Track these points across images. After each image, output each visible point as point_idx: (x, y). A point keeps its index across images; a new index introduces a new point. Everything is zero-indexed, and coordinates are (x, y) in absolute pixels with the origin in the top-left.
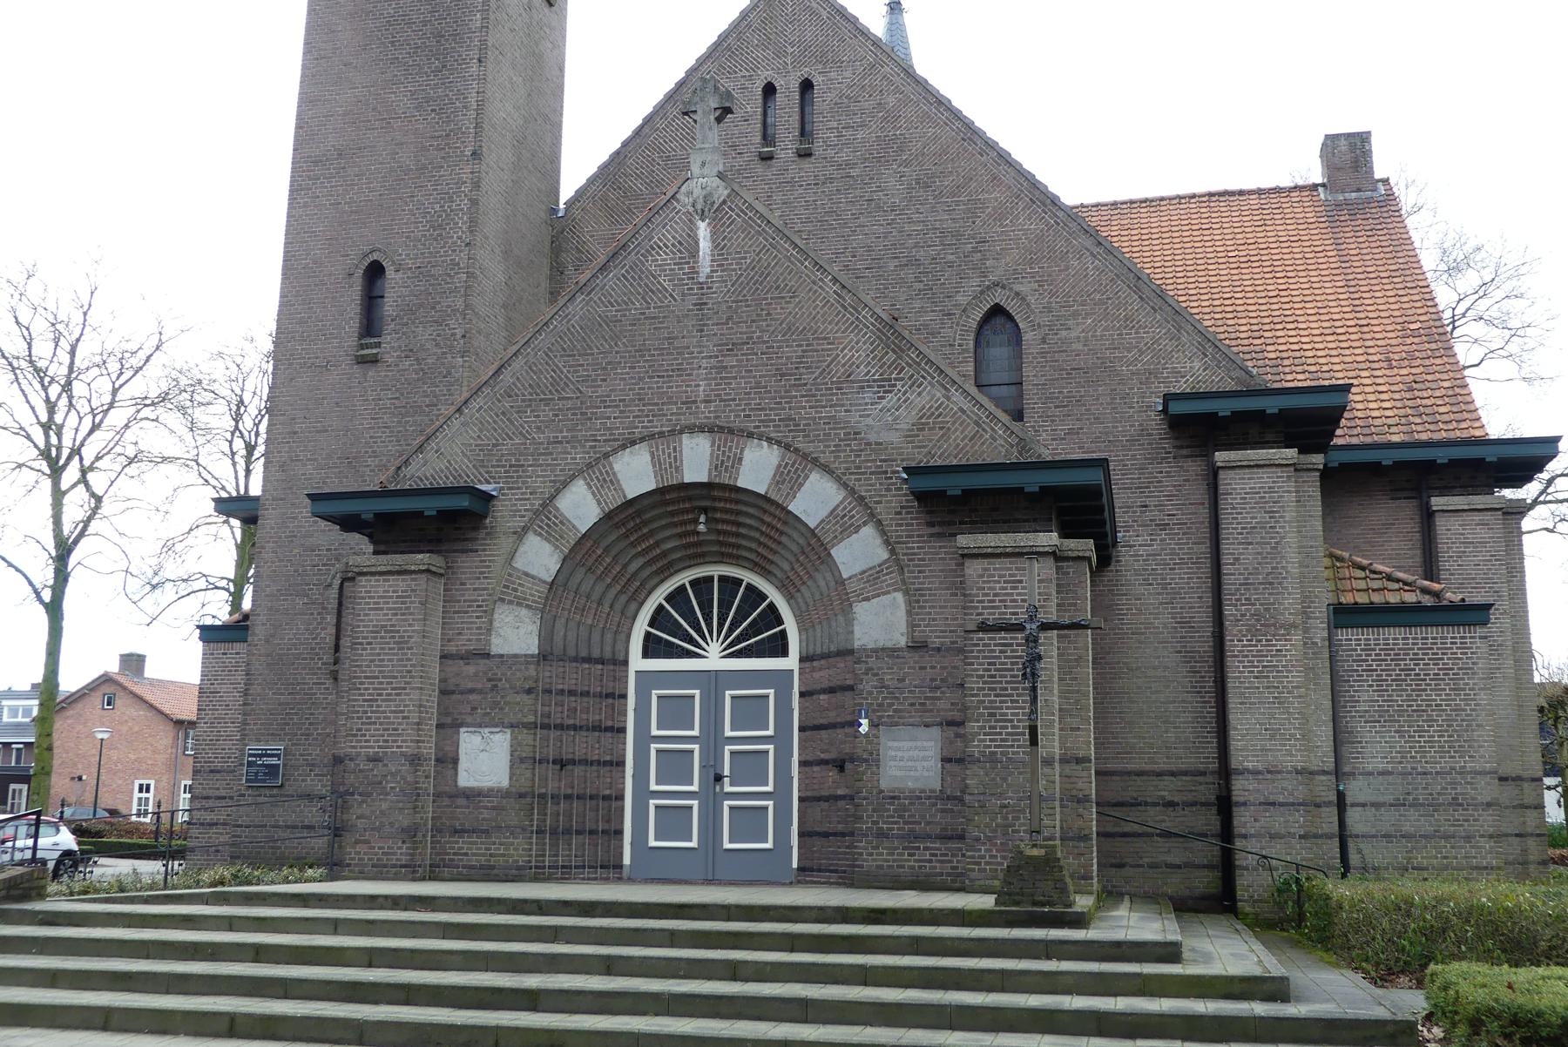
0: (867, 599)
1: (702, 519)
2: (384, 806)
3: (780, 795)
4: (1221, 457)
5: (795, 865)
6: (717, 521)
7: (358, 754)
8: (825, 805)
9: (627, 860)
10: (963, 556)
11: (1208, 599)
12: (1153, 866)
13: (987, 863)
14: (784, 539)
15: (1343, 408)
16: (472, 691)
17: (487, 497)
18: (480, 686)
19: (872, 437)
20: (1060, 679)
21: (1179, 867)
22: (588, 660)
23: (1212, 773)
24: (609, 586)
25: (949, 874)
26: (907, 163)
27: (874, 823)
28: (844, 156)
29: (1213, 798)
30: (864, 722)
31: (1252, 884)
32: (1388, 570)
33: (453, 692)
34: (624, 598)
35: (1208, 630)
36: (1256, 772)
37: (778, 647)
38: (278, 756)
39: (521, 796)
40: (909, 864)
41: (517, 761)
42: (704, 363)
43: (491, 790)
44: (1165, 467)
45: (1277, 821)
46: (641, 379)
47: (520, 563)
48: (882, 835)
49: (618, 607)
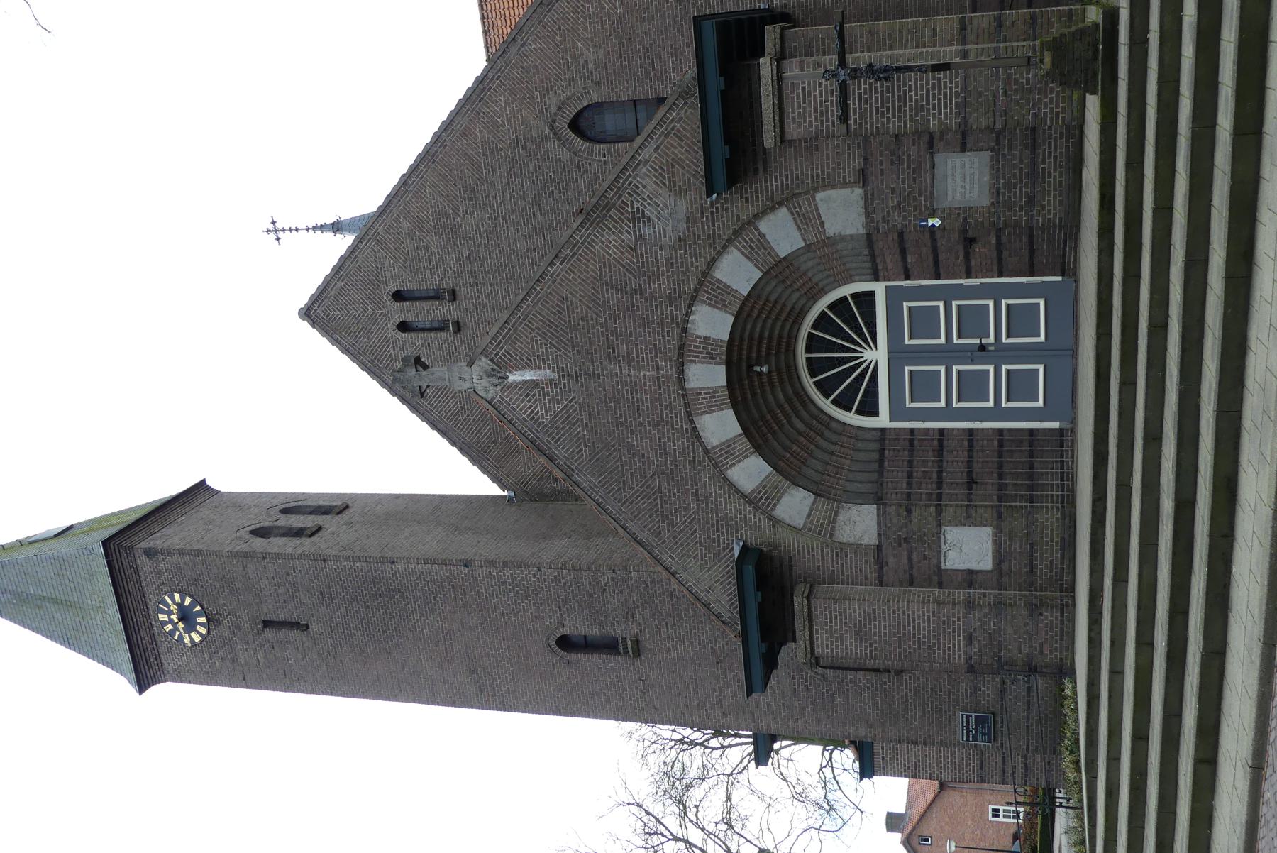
0: (822, 224)
1: (757, 369)
2: (1010, 631)
3: (996, 293)
5: (1059, 279)
6: (759, 356)
8: (1005, 254)
9: (1056, 425)
10: (782, 141)
13: (1057, 106)
14: (773, 298)
16: (910, 559)
17: (745, 549)
19: (683, 226)
20: (890, 49)
25: (1067, 141)
26: (456, 209)
27: (1021, 209)
28: (453, 262)
30: (930, 222)
33: (911, 575)
34: (827, 433)
37: (866, 300)
38: (968, 717)
39: (1000, 516)
41: (969, 520)
42: (626, 372)
43: (995, 542)
46: (641, 424)
47: (799, 521)
48: (1032, 201)
49: (834, 438)
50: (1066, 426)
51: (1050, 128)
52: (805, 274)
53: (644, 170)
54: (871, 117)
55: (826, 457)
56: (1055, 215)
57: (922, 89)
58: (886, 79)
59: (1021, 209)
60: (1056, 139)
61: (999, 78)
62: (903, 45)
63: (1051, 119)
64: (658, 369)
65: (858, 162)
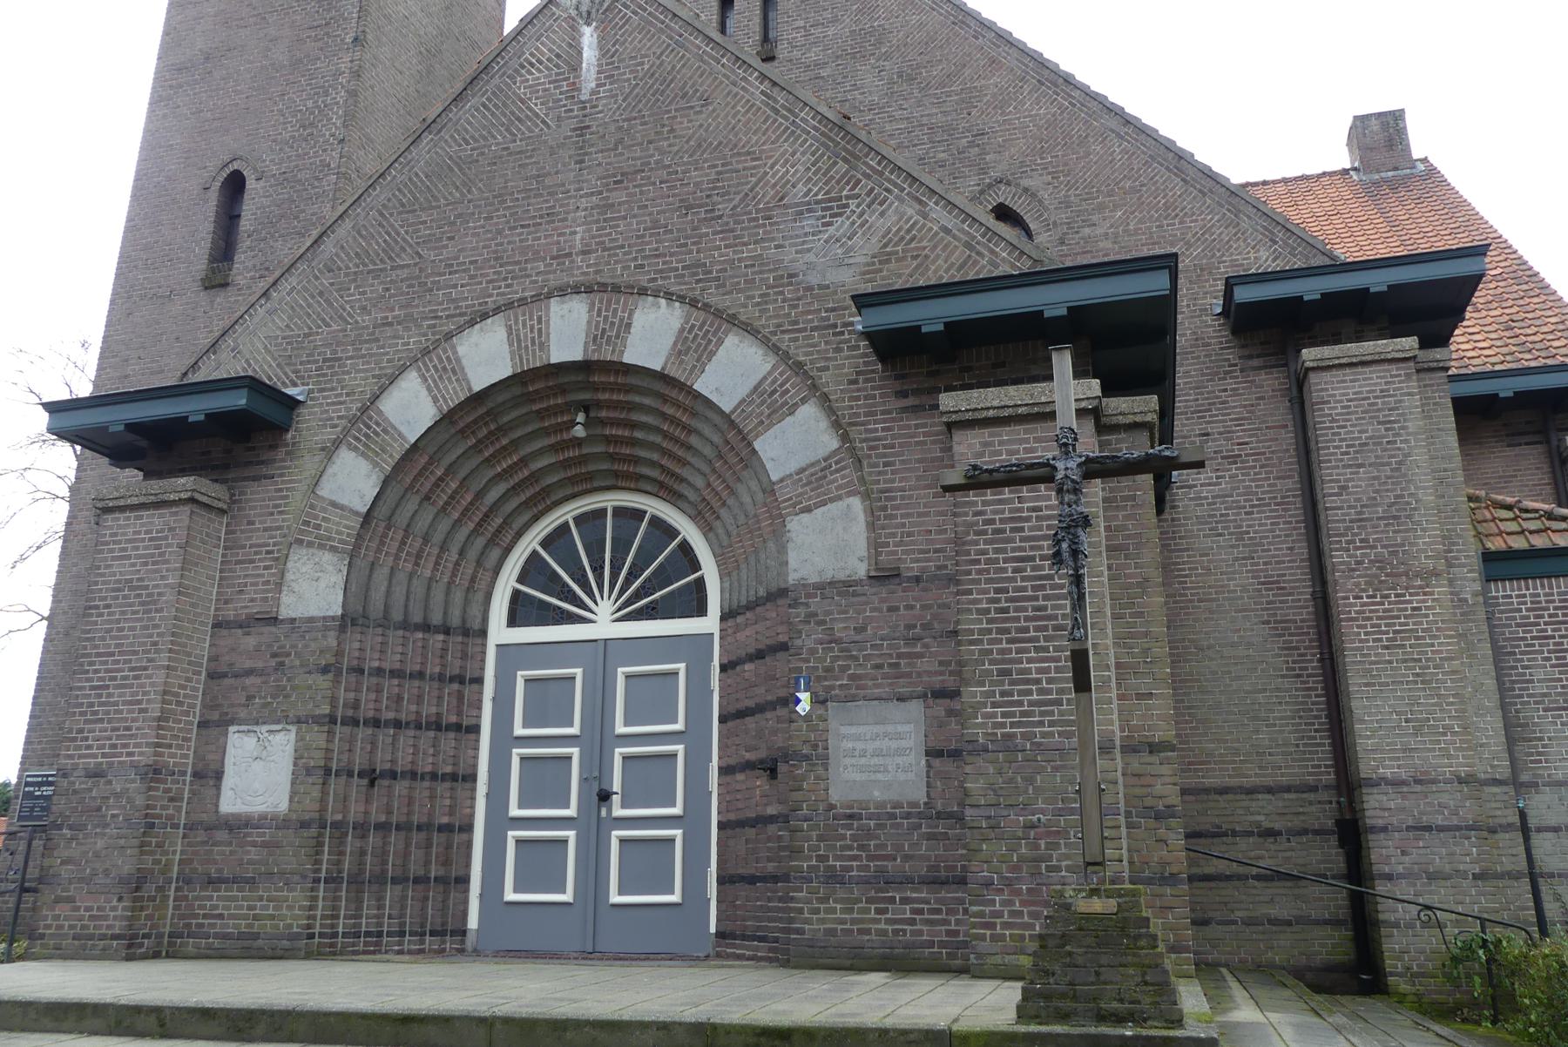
0: (808, 510)
1: (581, 418)
3: (692, 820)
4: (1309, 355)
5: (713, 930)
6: (603, 422)
7: (75, 767)
8: (751, 832)
9: (473, 922)
10: (950, 426)
11: (1302, 550)
12: (1250, 922)
13: (1006, 925)
14: (694, 440)
15: (1482, 276)
16: (250, 672)
17: (293, 403)
18: (260, 665)
19: (814, 279)
20: (1115, 617)
21: (1289, 923)
22: (426, 627)
23: (1326, 787)
24: (457, 523)
25: (942, 944)
26: (887, 56)
27: (821, 858)
28: (812, 56)
29: (1330, 823)
30: (805, 696)
31: (1407, 947)
32: (1546, 507)
33: (224, 675)
34: (480, 542)
35: (1305, 591)
36: (1397, 783)
39: (304, 825)
40: (880, 924)
41: (301, 771)
42: (583, 203)
43: (263, 817)
44: (1230, 383)
45: (1436, 853)
47: (326, 490)
48: (834, 878)
49: (472, 554)
50: (470, 940)
51: (966, 911)
52: (733, 493)
53: (910, 212)
54: (989, 581)
55: (438, 537)
56: (807, 921)
57: (1039, 670)
58: (1057, 558)
59: (821, 858)
60: (946, 922)
61: (1059, 813)
62: (1120, 641)
63: (981, 914)
64: (584, 253)
65: (911, 567)
